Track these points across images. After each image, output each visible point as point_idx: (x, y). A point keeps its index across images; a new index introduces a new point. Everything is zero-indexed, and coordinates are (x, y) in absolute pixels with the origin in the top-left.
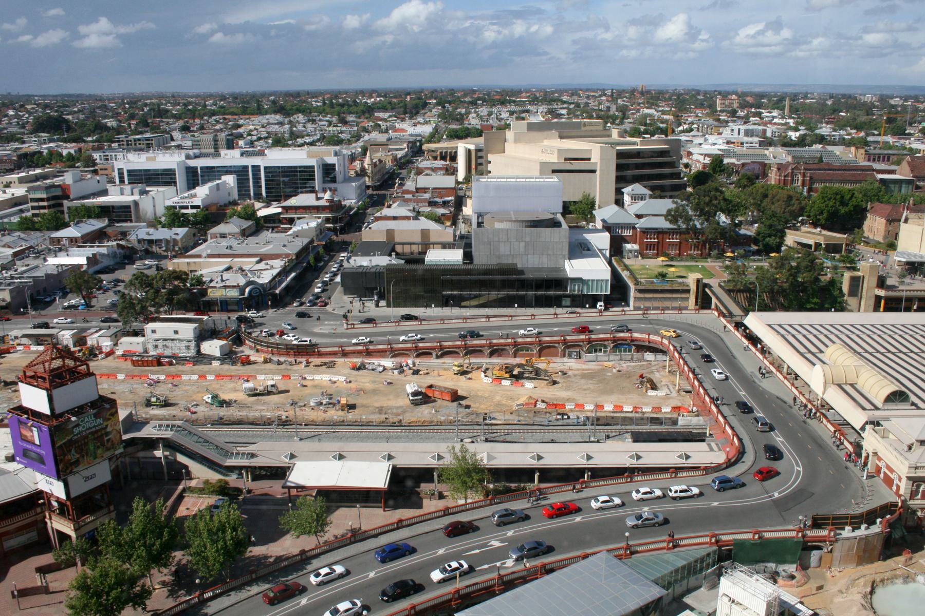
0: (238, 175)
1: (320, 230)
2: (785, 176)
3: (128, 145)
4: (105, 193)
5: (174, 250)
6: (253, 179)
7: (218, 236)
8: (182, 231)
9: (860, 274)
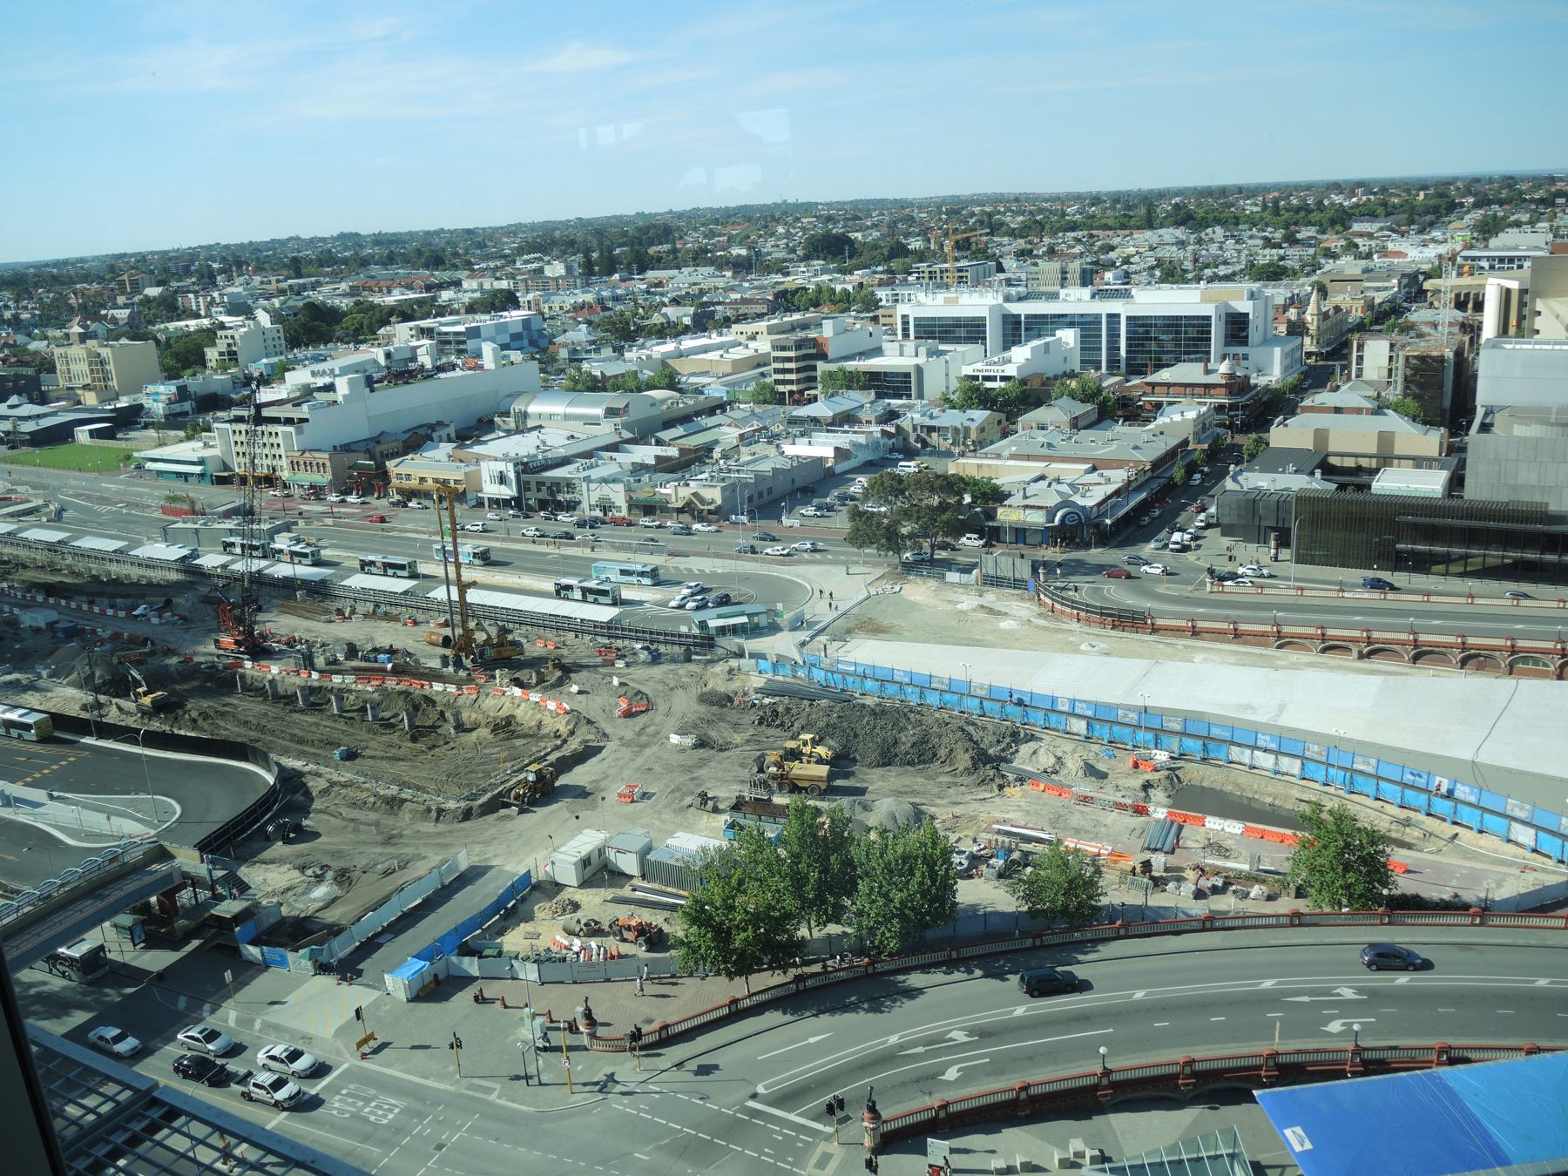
0: (1082, 330)
1: (1202, 425)
3: (930, 278)
4: (878, 351)
5: (964, 444)
6: (1108, 335)
7: (1034, 426)
8: (980, 415)
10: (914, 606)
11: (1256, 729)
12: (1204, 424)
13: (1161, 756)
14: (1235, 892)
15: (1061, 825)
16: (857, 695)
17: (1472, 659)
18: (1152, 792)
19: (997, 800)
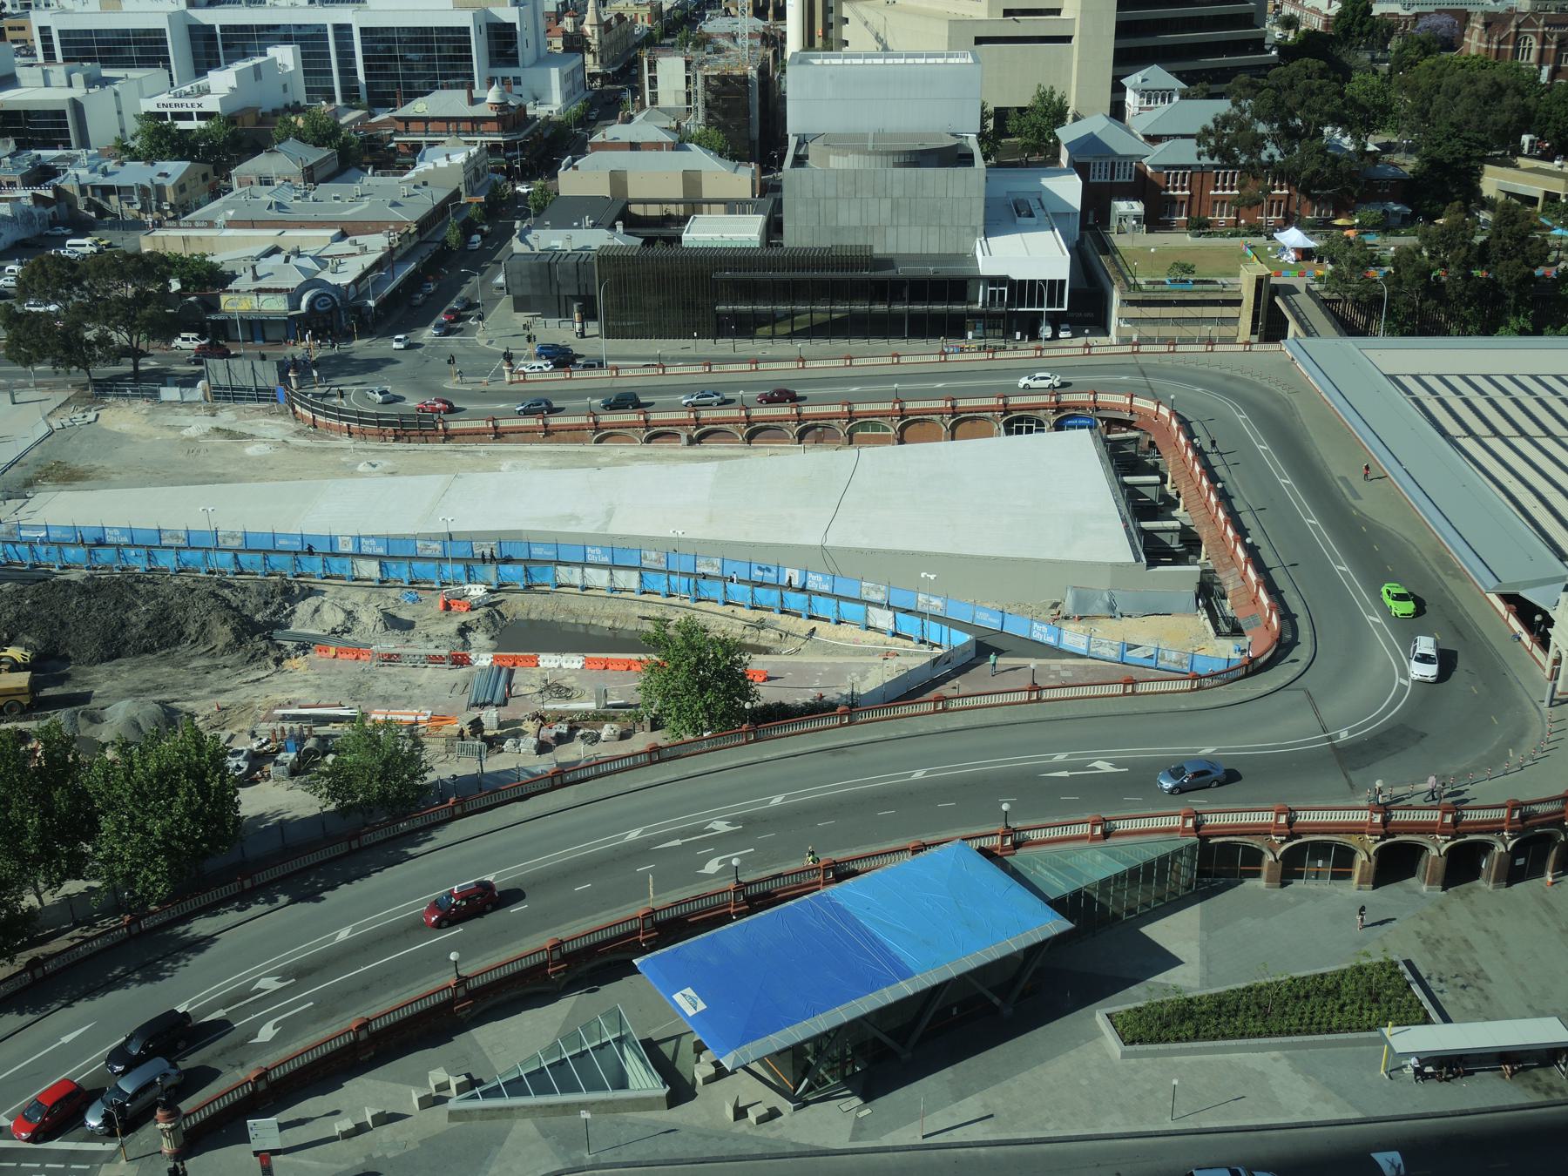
1: (474, 170)
2: (1500, 43)
5: (159, 209)
6: (339, 54)
7: (255, 180)
8: (176, 169)
10: (120, 438)
11: (584, 542)
12: (477, 170)
13: (477, 591)
14: (583, 737)
16: (55, 570)
18: (471, 636)
19: (275, 678)
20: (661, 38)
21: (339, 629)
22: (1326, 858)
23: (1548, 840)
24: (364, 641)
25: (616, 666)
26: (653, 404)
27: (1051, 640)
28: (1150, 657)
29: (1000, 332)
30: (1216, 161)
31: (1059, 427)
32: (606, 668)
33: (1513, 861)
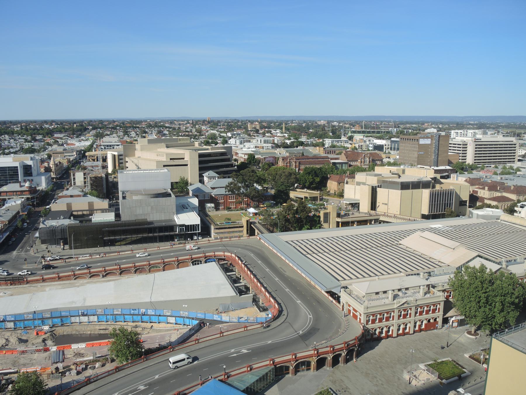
1: (23, 205)
2: (286, 164)
9: (328, 211)
11: (77, 309)
12: (24, 205)
13: (46, 328)
14: (90, 368)
15: (17, 365)
17: (138, 270)
18: (46, 342)
20: (71, 167)
21: (4, 345)
22: (304, 365)
23: (353, 350)
24: (13, 348)
25: (103, 344)
26: (91, 267)
27: (219, 319)
28: (246, 320)
29: (183, 239)
30: (230, 193)
31: (206, 262)
32: (93, 346)
33: (346, 357)
